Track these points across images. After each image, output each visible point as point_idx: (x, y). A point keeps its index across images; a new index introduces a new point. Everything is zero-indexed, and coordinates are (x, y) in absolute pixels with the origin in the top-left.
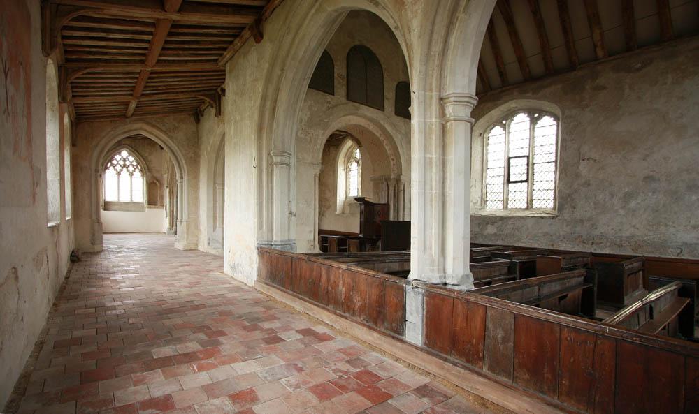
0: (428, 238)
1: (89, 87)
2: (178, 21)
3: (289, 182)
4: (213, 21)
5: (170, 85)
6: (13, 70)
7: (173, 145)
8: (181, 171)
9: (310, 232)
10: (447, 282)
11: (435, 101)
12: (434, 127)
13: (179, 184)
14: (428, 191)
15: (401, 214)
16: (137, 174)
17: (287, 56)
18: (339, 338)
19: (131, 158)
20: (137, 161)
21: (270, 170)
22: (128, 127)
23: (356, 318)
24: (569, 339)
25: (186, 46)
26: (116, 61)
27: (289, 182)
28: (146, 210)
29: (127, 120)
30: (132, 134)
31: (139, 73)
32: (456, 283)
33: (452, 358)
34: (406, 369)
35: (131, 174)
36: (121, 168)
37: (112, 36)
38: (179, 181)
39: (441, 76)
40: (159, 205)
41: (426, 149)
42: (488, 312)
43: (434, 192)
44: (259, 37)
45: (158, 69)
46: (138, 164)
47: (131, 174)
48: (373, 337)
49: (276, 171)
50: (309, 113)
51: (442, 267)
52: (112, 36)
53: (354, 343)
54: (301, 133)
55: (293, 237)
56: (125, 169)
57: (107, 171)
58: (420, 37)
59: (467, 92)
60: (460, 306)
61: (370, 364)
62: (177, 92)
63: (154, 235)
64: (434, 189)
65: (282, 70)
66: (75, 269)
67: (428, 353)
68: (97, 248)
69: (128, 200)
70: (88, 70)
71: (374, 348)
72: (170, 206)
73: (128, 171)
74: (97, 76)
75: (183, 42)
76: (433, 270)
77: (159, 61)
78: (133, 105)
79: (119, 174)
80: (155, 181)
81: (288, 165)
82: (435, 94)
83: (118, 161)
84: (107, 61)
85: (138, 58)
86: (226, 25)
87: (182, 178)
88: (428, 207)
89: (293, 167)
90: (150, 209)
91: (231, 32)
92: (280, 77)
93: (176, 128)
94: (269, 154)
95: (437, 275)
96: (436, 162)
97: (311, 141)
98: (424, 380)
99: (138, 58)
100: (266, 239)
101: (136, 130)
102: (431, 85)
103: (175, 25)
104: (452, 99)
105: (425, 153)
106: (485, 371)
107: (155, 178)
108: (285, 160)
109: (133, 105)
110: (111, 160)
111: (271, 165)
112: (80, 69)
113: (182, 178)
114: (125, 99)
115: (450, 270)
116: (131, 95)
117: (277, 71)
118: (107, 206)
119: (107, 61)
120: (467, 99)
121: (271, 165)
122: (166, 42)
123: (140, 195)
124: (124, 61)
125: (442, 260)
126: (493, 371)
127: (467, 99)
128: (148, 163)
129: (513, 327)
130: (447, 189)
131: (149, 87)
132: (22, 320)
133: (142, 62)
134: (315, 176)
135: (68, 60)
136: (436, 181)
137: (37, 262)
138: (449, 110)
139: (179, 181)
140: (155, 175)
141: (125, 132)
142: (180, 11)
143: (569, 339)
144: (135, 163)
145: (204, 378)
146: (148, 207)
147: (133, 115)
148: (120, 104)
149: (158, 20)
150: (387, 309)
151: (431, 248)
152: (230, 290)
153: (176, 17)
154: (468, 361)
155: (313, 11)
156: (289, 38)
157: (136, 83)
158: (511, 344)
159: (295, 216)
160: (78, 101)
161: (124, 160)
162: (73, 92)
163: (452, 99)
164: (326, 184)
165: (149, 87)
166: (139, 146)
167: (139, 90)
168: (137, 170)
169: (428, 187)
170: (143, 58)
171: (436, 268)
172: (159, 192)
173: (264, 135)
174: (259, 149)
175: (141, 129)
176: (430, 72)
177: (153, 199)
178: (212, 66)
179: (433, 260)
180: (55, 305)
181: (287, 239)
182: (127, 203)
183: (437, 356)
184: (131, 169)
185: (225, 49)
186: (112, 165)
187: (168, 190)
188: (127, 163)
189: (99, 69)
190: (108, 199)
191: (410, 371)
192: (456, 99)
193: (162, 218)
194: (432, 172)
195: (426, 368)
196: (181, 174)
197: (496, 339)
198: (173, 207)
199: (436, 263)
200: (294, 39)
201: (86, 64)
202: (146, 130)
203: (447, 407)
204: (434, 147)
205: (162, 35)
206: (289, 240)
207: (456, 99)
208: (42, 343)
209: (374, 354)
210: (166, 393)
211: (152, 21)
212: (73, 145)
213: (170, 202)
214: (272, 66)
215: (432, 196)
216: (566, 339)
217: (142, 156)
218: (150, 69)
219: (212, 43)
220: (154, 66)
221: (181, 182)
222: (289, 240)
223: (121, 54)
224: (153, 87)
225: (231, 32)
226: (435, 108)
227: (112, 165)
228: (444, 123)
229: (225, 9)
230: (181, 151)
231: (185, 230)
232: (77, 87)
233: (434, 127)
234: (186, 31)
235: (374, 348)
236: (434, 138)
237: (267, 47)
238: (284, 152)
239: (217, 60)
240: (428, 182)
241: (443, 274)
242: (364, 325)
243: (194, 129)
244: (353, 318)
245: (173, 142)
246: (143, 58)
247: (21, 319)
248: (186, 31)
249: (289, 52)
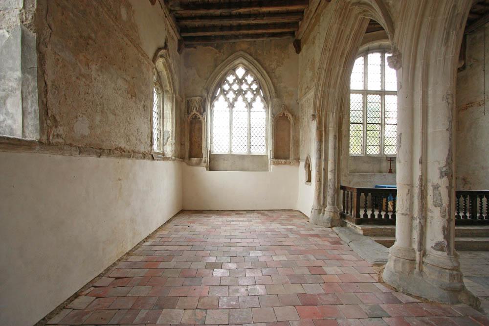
28: (272, 167)
35: (249, 106)
36: (234, 96)
40: (292, 157)
46: (260, 87)
47: (249, 106)
56: (240, 98)
69: (243, 151)
72: (320, 158)
80: (286, 113)
83: (230, 85)
107: (286, 108)
110: (220, 84)
118: (213, 163)
123: (262, 146)
128: (275, 80)
130: (228, 140)
140: (286, 103)
146: (275, 163)
168: (258, 99)
172: (292, 133)
180: (127, 13)
182: (242, 157)
184: (249, 96)
186: (223, 91)
187: (314, 125)
188: (244, 87)
190: (216, 151)
198: (326, 160)
203: (27, 94)
213: (320, 150)
217: (265, 69)
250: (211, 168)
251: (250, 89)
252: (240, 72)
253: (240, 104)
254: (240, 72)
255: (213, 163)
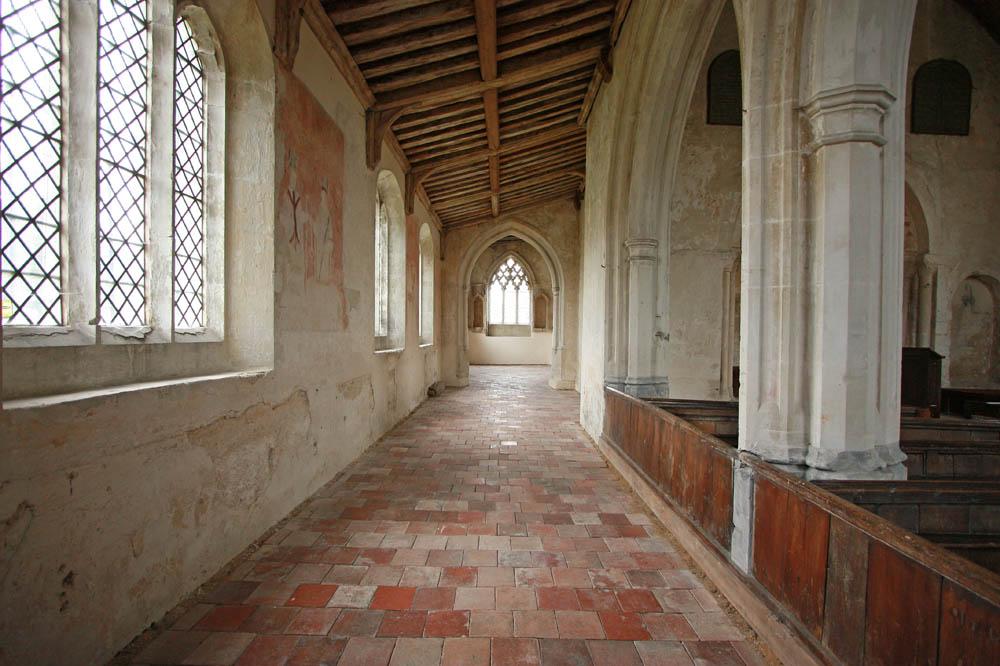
0: (769, 375)
1: (443, 190)
2: (504, 86)
3: (655, 285)
4: (543, 72)
5: (530, 167)
6: (307, 197)
7: (547, 243)
8: (557, 279)
9: (715, 366)
10: (808, 462)
11: (784, 117)
12: (782, 165)
13: (555, 298)
14: (770, 287)
15: (926, 334)
16: (524, 287)
17: (641, 89)
18: (655, 537)
19: (518, 267)
20: (524, 272)
21: (625, 269)
22: (497, 228)
23: (682, 510)
24: (955, 612)
25: (528, 114)
26: (459, 154)
27: (655, 285)
28: (533, 334)
29: (496, 220)
30: (501, 237)
31: (487, 161)
32: (823, 465)
33: (780, 606)
34: (719, 609)
37: (443, 127)
38: (555, 293)
39: (798, 67)
41: (765, 208)
42: (832, 527)
43: (781, 287)
44: (609, 70)
45: (504, 150)
48: (694, 544)
49: (633, 271)
50: (714, 167)
51: (800, 432)
52: (443, 127)
53: (671, 550)
54: (699, 203)
55: (660, 373)
57: (492, 286)
58: (752, 9)
59: (852, 83)
60: (796, 508)
61: (664, 585)
62: (543, 173)
63: (538, 368)
64: (781, 281)
65: (636, 113)
66: (428, 403)
67: (754, 589)
68: (463, 382)
69: (914, 346)
70: (432, 172)
71: (692, 565)
73: (514, 283)
74: (446, 175)
75: (525, 109)
76: (778, 436)
77: (502, 142)
78: (495, 201)
79: (504, 288)
81: (655, 260)
82: (785, 103)
84: (449, 156)
85: (480, 143)
86: (568, 70)
87: (558, 289)
88: (770, 314)
89: (664, 261)
90: (536, 334)
91: (580, 76)
92: (634, 125)
93: (552, 221)
94: (624, 245)
95: (785, 446)
96: (786, 230)
97: (717, 214)
98: (733, 634)
99: (480, 143)
100: (616, 375)
101: (506, 231)
102: (778, 88)
103: (502, 93)
104: (818, 105)
105: (764, 216)
106: (824, 645)
108: (651, 252)
109: (495, 201)
110: (495, 273)
111: (626, 262)
112: (425, 172)
113: (558, 289)
114: (484, 196)
115: (816, 440)
116: (489, 189)
117: (629, 118)
118: (491, 331)
119: (449, 156)
120: (852, 97)
121: (626, 262)
122: (501, 116)
123: (526, 318)
124: (466, 151)
125: (800, 419)
126: (835, 650)
127: (852, 97)
129: (866, 565)
131: (506, 175)
132: (315, 444)
133: (486, 146)
134: (725, 272)
135: (414, 165)
136: (785, 268)
137: (348, 389)
138: (819, 126)
139: (555, 293)
141: (492, 237)
142: (499, 74)
143: (955, 612)
144: (521, 274)
145: (439, 542)
147: (500, 213)
148: (480, 202)
149: (483, 93)
150: (715, 499)
151: (774, 394)
152: (565, 447)
153: (499, 83)
154: (804, 620)
155: (665, 11)
156: (640, 62)
157: (489, 173)
158: (862, 600)
159: (667, 338)
160: (439, 207)
161: (510, 270)
162: (430, 198)
163: (818, 105)
164: (947, 285)
165: (506, 175)
166: (523, 252)
167: (495, 184)
168: (524, 282)
169: (769, 279)
170: (485, 142)
171: (783, 433)
173: (617, 217)
174: (610, 238)
175: (511, 229)
176: (775, 66)
177: (540, 322)
178: (572, 129)
179: (776, 416)
181: (649, 375)
183: (763, 598)
184: (517, 281)
185: (581, 102)
186: (497, 277)
188: (514, 274)
189: (444, 167)
190: (493, 321)
191: (722, 613)
192: (826, 103)
193: (547, 341)
194: (778, 251)
195: (746, 615)
196: (557, 283)
197: (840, 583)
199: (784, 422)
200: (645, 64)
201: (428, 166)
202: (516, 230)
204: (782, 203)
205: (491, 105)
206: (653, 378)
207: (826, 103)
208: (343, 474)
209: (687, 573)
210: (394, 547)
211: (478, 97)
212: (442, 256)
214: (621, 111)
215: (778, 294)
216: (951, 612)
218: (495, 154)
219: (560, 98)
220: (499, 148)
221: (558, 295)
222: (653, 378)
223: (461, 144)
224: (509, 173)
225: (580, 76)
226: (784, 129)
227: (498, 278)
228: (808, 153)
229: (557, 51)
230: (556, 252)
231: (560, 362)
232: (433, 192)
233: (782, 165)
234: (519, 95)
235: (692, 565)
236: (782, 185)
237: (616, 82)
238: (643, 240)
239: (576, 118)
240: (770, 270)
241: (801, 447)
242: (689, 523)
243: (574, 218)
244: (679, 508)
245: (547, 240)
246: (485, 142)
247: (312, 443)
248: (519, 95)
249: (641, 83)
250: (489, 335)
251: (518, 275)
252: (511, 262)
253: (510, 287)
254: (511, 262)
255: (491, 331)
